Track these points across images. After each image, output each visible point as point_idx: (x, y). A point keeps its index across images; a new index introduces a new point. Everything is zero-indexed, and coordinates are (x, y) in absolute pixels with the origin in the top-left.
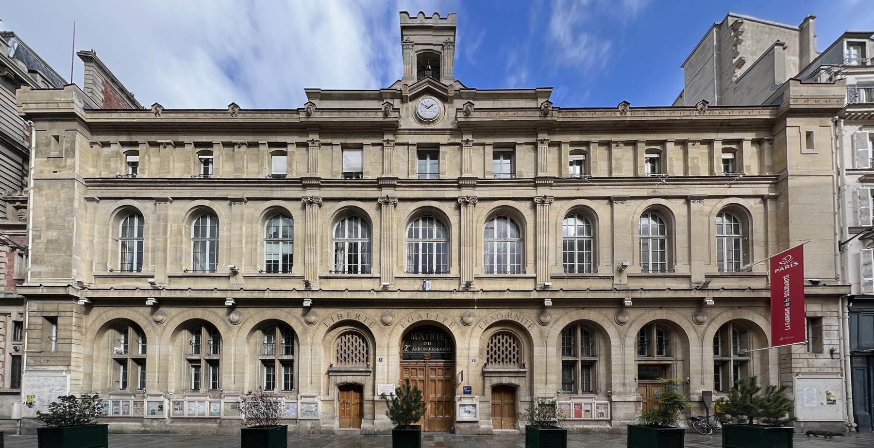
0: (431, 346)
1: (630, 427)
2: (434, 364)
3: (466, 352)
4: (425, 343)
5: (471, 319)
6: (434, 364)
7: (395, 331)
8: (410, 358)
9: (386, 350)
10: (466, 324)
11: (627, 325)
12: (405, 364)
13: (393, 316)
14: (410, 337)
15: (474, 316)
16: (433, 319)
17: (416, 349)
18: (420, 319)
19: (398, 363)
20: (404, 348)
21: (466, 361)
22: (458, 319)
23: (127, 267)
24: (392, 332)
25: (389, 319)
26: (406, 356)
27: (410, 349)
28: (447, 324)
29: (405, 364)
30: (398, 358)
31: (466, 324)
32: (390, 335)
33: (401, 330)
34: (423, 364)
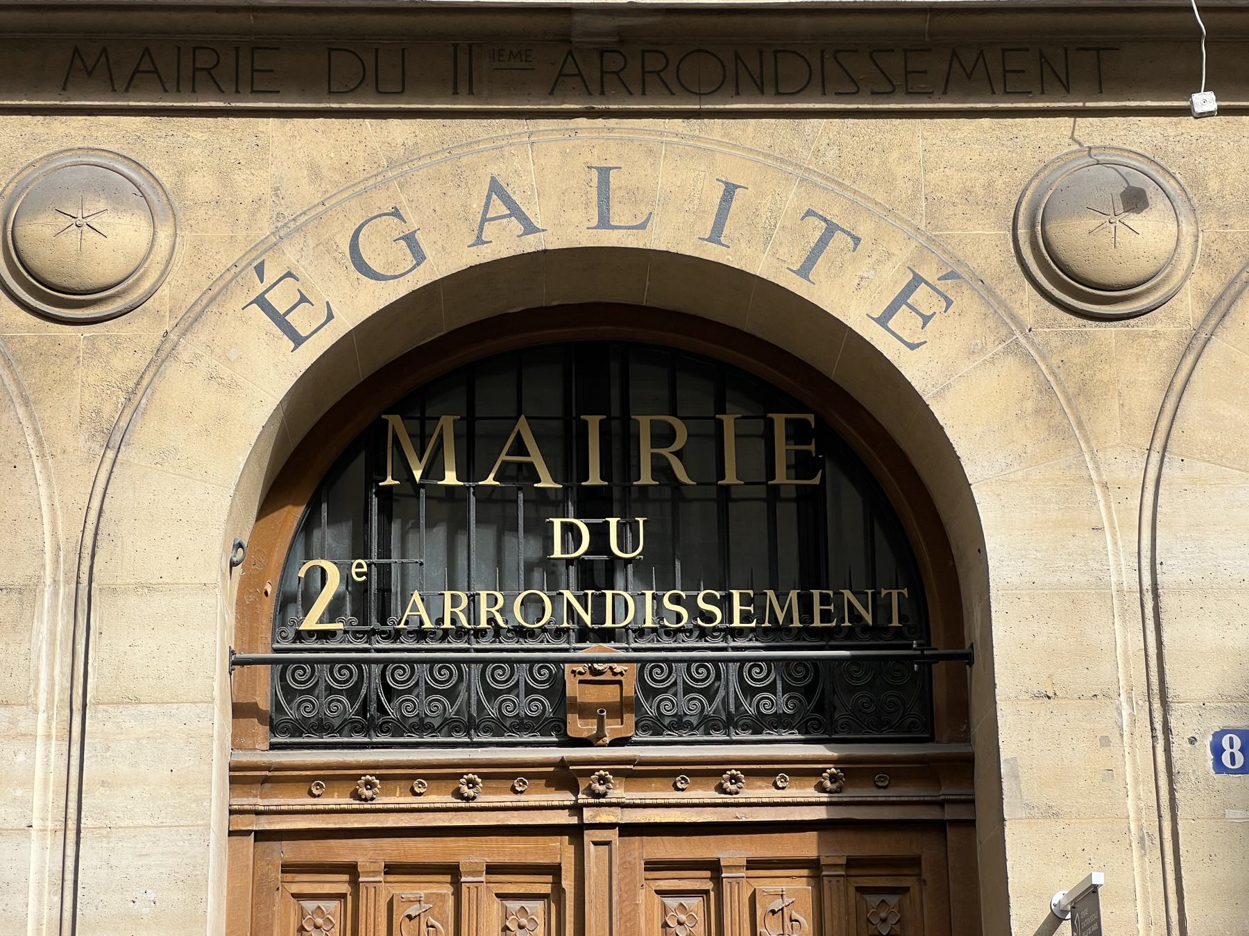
0: (654, 569)
1: (620, 836)
2: (697, 801)
3: (1127, 637)
4: (570, 534)
5: (1144, 239)
6: (697, 801)
7: (179, 383)
8: (370, 721)
9: (50, 620)
10: (1086, 294)
11: (1166, 328)
12: (290, 807)
13: (151, 197)
14: (373, 448)
15: (1189, 202)
16: (674, 232)
17: (456, 598)
18: (505, 243)
19: (215, 797)
20: (292, 600)
21: (1135, 761)
22: (987, 243)
23: (473, 892)
24: (137, 393)
25: (107, 241)
26: (312, 697)
27: (371, 602)
28: (850, 296)
29: (290, 807)
30: (217, 721)
31: (1086, 294)
32: (114, 440)
33: (253, 380)
34: (549, 805)
